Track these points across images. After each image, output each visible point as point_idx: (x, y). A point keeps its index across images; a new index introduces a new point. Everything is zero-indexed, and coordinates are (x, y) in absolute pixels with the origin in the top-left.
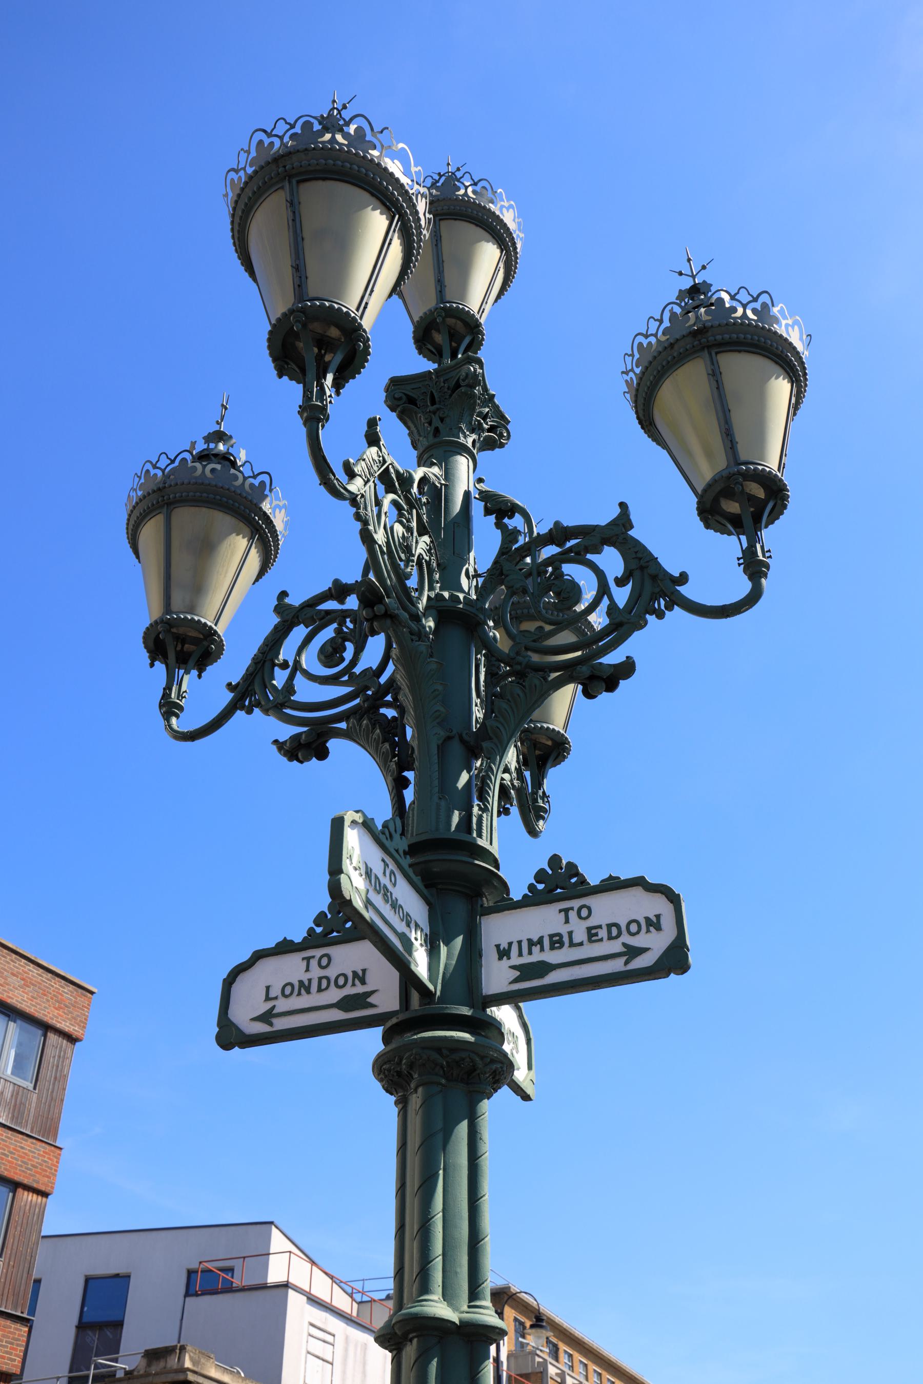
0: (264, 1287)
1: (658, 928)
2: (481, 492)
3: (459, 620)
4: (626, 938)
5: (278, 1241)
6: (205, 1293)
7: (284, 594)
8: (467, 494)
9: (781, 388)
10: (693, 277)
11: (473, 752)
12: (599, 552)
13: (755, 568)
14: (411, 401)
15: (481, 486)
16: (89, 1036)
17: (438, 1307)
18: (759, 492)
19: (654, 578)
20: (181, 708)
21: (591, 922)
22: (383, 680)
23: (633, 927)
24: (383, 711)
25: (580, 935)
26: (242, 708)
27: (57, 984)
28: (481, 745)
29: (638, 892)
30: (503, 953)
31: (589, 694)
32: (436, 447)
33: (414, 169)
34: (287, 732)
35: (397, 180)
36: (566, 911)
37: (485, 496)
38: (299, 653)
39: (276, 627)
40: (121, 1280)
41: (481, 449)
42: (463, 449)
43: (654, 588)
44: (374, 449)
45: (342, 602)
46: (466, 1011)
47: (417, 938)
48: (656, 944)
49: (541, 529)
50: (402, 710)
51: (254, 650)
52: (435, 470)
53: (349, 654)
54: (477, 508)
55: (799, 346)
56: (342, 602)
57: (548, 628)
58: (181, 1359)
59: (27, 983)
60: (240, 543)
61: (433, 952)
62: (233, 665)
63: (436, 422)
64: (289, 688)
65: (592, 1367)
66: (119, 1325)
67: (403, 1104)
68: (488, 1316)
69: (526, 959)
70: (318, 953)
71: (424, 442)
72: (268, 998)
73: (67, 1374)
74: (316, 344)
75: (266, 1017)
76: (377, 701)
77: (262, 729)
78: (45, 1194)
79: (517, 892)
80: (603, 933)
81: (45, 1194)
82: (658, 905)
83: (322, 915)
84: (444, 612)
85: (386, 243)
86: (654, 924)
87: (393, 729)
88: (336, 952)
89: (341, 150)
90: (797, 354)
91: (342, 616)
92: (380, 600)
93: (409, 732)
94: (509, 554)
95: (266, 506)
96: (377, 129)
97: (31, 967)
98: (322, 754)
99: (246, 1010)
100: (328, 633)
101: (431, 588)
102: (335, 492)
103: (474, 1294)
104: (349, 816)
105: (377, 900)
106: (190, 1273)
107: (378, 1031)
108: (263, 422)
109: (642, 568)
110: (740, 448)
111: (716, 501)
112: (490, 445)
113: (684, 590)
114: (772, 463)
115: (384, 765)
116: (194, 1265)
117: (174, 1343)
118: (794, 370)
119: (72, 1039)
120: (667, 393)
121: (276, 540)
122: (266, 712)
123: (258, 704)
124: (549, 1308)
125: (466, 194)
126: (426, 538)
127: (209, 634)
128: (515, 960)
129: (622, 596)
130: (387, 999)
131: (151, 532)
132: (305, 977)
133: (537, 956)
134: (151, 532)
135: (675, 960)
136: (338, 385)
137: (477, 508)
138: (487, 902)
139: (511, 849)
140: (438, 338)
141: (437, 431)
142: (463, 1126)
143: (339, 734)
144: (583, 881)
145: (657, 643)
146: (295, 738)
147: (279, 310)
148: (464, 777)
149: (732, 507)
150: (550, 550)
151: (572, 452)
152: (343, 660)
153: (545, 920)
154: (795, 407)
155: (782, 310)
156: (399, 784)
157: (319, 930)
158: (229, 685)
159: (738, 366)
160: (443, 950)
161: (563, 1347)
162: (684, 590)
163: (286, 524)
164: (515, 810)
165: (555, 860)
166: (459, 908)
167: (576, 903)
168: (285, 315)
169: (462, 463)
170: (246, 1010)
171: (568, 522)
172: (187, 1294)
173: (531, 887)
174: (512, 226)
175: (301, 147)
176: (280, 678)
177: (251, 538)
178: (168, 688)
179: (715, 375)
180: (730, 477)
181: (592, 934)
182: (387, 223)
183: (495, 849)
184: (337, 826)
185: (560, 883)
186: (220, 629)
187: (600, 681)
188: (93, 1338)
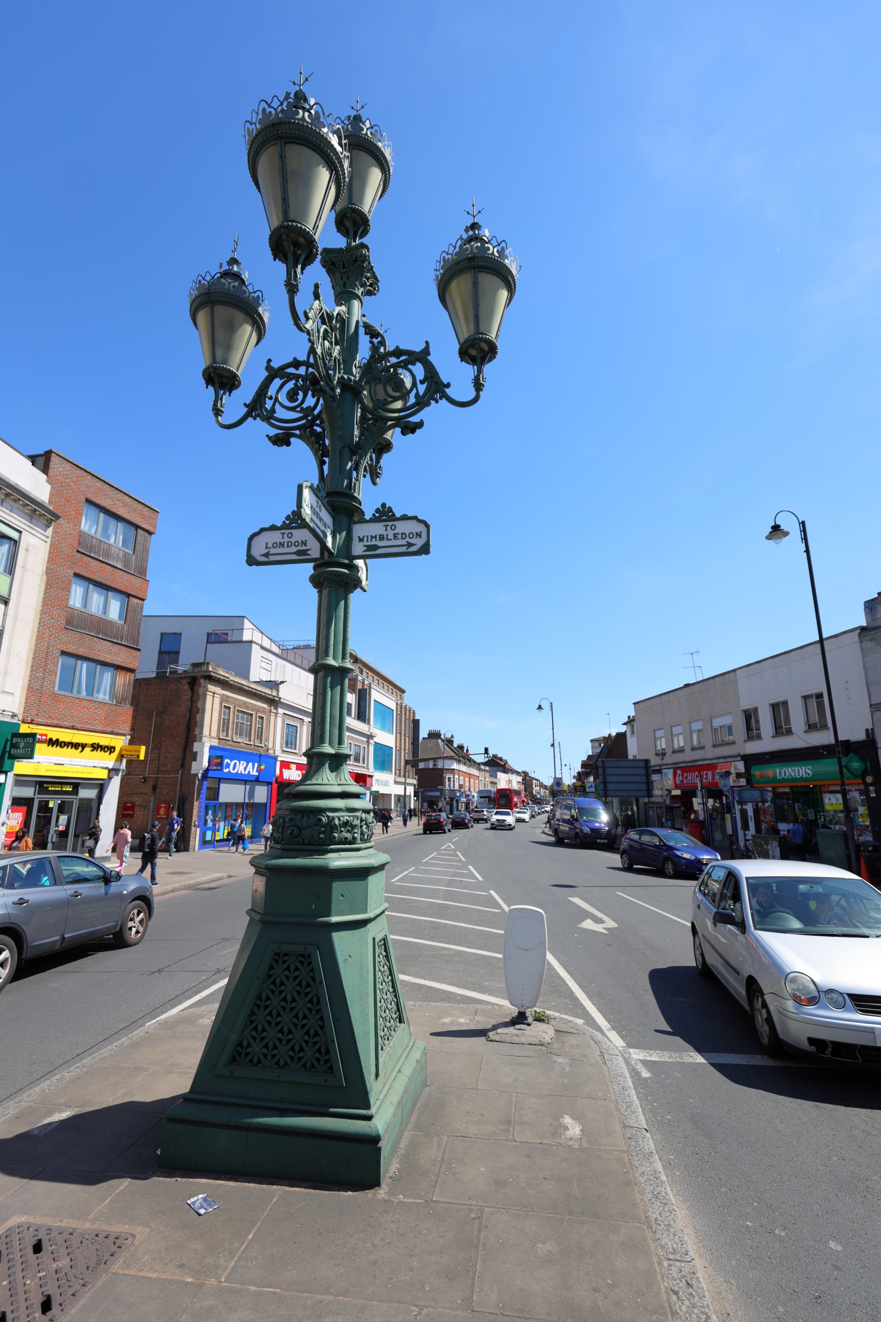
0: (242, 642)
1: (420, 537)
2: (364, 323)
3: (351, 390)
4: (408, 539)
5: (247, 624)
6: (216, 642)
7: (269, 361)
8: (357, 322)
9: (504, 294)
10: (474, 217)
11: (353, 453)
12: (414, 364)
13: (478, 386)
14: (333, 264)
15: (364, 319)
16: (158, 531)
17: (331, 661)
18: (486, 348)
19: (436, 383)
20: (222, 412)
21: (395, 532)
22: (316, 412)
23: (411, 536)
24: (315, 428)
25: (391, 536)
26: (252, 416)
27: (140, 507)
28: (356, 451)
29: (414, 521)
30: (361, 540)
31: (404, 433)
32: (344, 295)
33: (344, 142)
34: (273, 432)
35: (335, 149)
36: (386, 526)
37: (367, 326)
38: (277, 393)
39: (266, 378)
40: (178, 636)
41: (366, 295)
42: (356, 297)
43: (436, 387)
44: (317, 302)
45: (297, 369)
46: (347, 562)
47: (329, 533)
48: (419, 543)
49: (390, 347)
50: (324, 429)
51: (256, 388)
52: (343, 308)
53: (300, 396)
54: (362, 330)
55: (514, 272)
56: (297, 369)
57: (389, 399)
58: (207, 667)
59: (125, 505)
60: (248, 328)
61: (334, 537)
62: (246, 393)
63: (345, 279)
64: (273, 410)
65: (376, 677)
66: (178, 653)
67: (320, 593)
68: (348, 664)
69: (370, 543)
70: (287, 531)
71: (339, 289)
72: (267, 548)
73: (155, 669)
74: (291, 245)
75: (266, 555)
76: (312, 424)
77: (259, 429)
78: (143, 600)
79: (368, 516)
80: (399, 536)
81: (143, 600)
82: (421, 528)
83: (289, 516)
84: (345, 385)
85: (328, 188)
86: (419, 535)
87: (320, 437)
88: (295, 532)
89: (307, 126)
90: (513, 277)
91: (297, 377)
92: (319, 383)
93: (327, 442)
94: (376, 356)
95: (260, 310)
96: (326, 114)
97: (126, 497)
98: (288, 444)
99: (258, 551)
100: (290, 385)
101: (339, 373)
102: (300, 328)
103: (344, 658)
104: (305, 484)
105: (315, 518)
106: (208, 634)
107: (311, 565)
108: (264, 274)
109: (432, 377)
110: (481, 325)
111: (467, 349)
112: (370, 293)
113: (448, 391)
114: (492, 336)
115: (315, 454)
116: (211, 631)
117: (202, 661)
118: (511, 288)
119: (150, 533)
120: (454, 285)
121: (265, 328)
122: (263, 420)
123: (259, 416)
124: (361, 656)
125: (366, 134)
126: (338, 347)
127: (234, 376)
128: (365, 543)
129: (422, 389)
130: (315, 553)
131: (202, 316)
132: (282, 541)
133: (374, 542)
134: (202, 316)
135: (425, 550)
136: (303, 269)
137: (362, 330)
138: (356, 519)
139: (368, 496)
140: (348, 223)
141: (345, 283)
142: (342, 603)
143: (295, 436)
144: (394, 515)
145: (435, 414)
146: (277, 435)
147: (275, 224)
148: (350, 464)
149: (473, 352)
150: (393, 360)
151: (406, 311)
152: (297, 400)
153: (377, 529)
154: (508, 304)
155: (510, 253)
156: (321, 463)
157: (287, 522)
158: (245, 404)
159: (488, 280)
160: (338, 536)
161: (364, 670)
162: (448, 391)
163: (269, 319)
164: (368, 476)
165: (384, 505)
166: (345, 520)
167: (390, 523)
168: (278, 227)
169: (356, 304)
170: (258, 551)
171: (403, 347)
172: (207, 643)
173: (374, 515)
174: (389, 158)
175: (287, 120)
176: (269, 404)
177: (253, 326)
178: (216, 401)
179: (475, 284)
180: (475, 339)
181: (395, 536)
182: (329, 176)
183: (360, 497)
184: (300, 488)
185: (385, 514)
186: (239, 374)
187: (410, 429)
188: (166, 657)
